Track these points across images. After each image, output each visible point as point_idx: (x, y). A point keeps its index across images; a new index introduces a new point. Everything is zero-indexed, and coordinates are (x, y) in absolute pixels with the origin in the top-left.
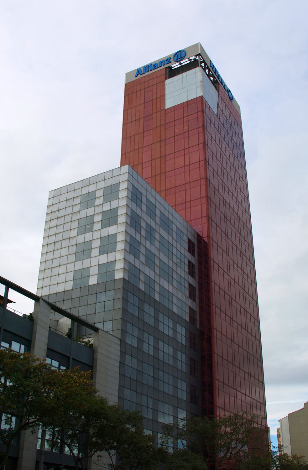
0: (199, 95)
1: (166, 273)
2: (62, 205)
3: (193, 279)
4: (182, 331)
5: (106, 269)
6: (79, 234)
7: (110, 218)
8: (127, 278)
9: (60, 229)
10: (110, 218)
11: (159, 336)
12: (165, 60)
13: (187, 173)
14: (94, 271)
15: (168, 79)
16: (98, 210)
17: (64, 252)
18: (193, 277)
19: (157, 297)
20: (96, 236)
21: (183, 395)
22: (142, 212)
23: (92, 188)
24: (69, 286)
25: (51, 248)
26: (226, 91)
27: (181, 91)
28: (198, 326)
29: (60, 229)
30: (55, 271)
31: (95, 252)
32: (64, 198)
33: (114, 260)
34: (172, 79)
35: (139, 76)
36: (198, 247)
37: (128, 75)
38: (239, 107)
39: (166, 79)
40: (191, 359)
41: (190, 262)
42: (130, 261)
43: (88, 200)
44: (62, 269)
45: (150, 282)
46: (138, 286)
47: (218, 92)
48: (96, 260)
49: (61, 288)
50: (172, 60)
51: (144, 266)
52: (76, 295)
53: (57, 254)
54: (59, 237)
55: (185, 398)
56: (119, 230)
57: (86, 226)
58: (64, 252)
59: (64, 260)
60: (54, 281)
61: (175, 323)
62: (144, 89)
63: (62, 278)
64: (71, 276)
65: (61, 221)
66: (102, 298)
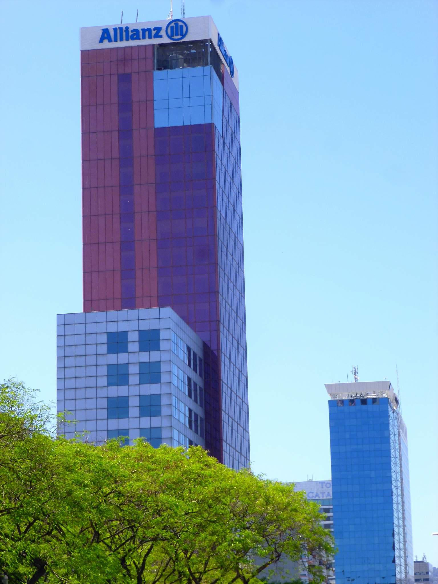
6: (109, 384)
12: (152, 28)
16: (134, 358)
35: (107, 45)
39: (154, 70)
50: (163, 33)
57: (118, 375)
59: (92, 414)
65: (81, 361)
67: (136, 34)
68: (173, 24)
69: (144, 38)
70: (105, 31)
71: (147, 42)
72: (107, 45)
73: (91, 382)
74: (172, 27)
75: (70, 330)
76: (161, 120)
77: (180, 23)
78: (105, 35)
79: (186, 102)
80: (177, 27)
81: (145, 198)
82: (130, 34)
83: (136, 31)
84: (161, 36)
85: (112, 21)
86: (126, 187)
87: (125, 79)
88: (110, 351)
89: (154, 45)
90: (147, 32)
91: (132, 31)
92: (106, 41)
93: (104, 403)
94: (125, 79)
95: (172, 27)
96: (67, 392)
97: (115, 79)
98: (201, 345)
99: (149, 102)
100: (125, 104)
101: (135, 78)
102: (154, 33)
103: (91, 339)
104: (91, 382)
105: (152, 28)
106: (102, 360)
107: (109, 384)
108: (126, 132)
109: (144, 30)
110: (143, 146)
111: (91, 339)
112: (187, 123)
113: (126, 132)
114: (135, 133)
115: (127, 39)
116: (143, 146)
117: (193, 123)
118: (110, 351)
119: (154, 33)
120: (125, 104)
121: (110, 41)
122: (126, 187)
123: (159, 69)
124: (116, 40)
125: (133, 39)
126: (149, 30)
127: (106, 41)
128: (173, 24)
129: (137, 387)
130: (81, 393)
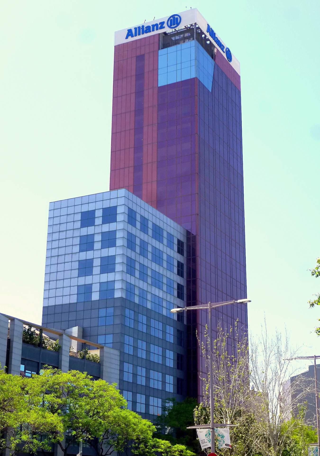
0: (193, 76)
1: (157, 282)
2: (64, 219)
3: (181, 256)
4: (170, 330)
5: (107, 289)
6: (81, 251)
7: (109, 240)
8: (124, 297)
9: (62, 243)
10: (109, 240)
11: (149, 339)
12: (158, 23)
13: (179, 72)
14: (96, 288)
15: (162, 49)
16: (98, 230)
17: (68, 266)
18: (181, 254)
19: (149, 306)
20: (97, 254)
21: (170, 363)
22: (136, 231)
23: (91, 207)
24: (74, 299)
25: (54, 260)
26: (224, 53)
27: (175, 67)
28: (185, 323)
29: (62, 243)
30: (60, 284)
31: (96, 270)
32: (64, 212)
33: (113, 280)
34: (165, 49)
35: (130, 39)
36: (187, 289)
37: (117, 34)
38: (238, 78)
39: (159, 49)
40: (178, 330)
41: (179, 285)
42: (127, 281)
43: (88, 219)
44: (67, 283)
45: (143, 294)
46: (133, 301)
47: (215, 60)
48: (97, 279)
49: (66, 301)
50: (165, 25)
51: (138, 280)
52: (80, 307)
53: (61, 267)
54: (62, 251)
55: (172, 391)
56: (117, 251)
57: (87, 243)
58: (68, 266)
59: (68, 274)
60: (59, 292)
61: (164, 324)
62: (136, 58)
63: (67, 291)
64: (75, 290)
65: (63, 235)
66: (102, 313)
67: (148, 29)
68: (172, 18)
69: (153, 30)
70: (130, 31)
71: (156, 32)
72: (130, 39)
73: (69, 250)
74: (171, 20)
75: (57, 213)
76: (162, 81)
77: (176, 17)
78: (130, 33)
79: (179, 66)
80: (174, 20)
81: (150, 134)
82: (145, 29)
83: (148, 27)
84: (164, 27)
85: (133, 25)
86: (138, 129)
87: (140, 58)
88: (82, 226)
89: (159, 34)
90: (156, 26)
91: (146, 28)
92: (130, 37)
93: (76, 265)
94: (140, 58)
95: (171, 20)
96: (53, 258)
97: (134, 60)
98: (184, 232)
99: (155, 71)
100: (140, 75)
101: (146, 57)
102: (159, 26)
103: (70, 218)
104: (69, 250)
105: (158, 23)
106: (77, 233)
107: (81, 251)
108: (140, 93)
109: (153, 26)
110: (150, 100)
111: (70, 218)
112: (179, 80)
113: (140, 93)
114: (146, 93)
115: (143, 33)
116: (150, 100)
117: (183, 79)
118: (82, 226)
119: (159, 26)
120: (140, 75)
121: (132, 36)
122: (138, 129)
123: (163, 48)
124: (136, 35)
125: (146, 32)
126: (157, 25)
127: (130, 37)
128: (172, 18)
129: (100, 251)
130: (61, 259)
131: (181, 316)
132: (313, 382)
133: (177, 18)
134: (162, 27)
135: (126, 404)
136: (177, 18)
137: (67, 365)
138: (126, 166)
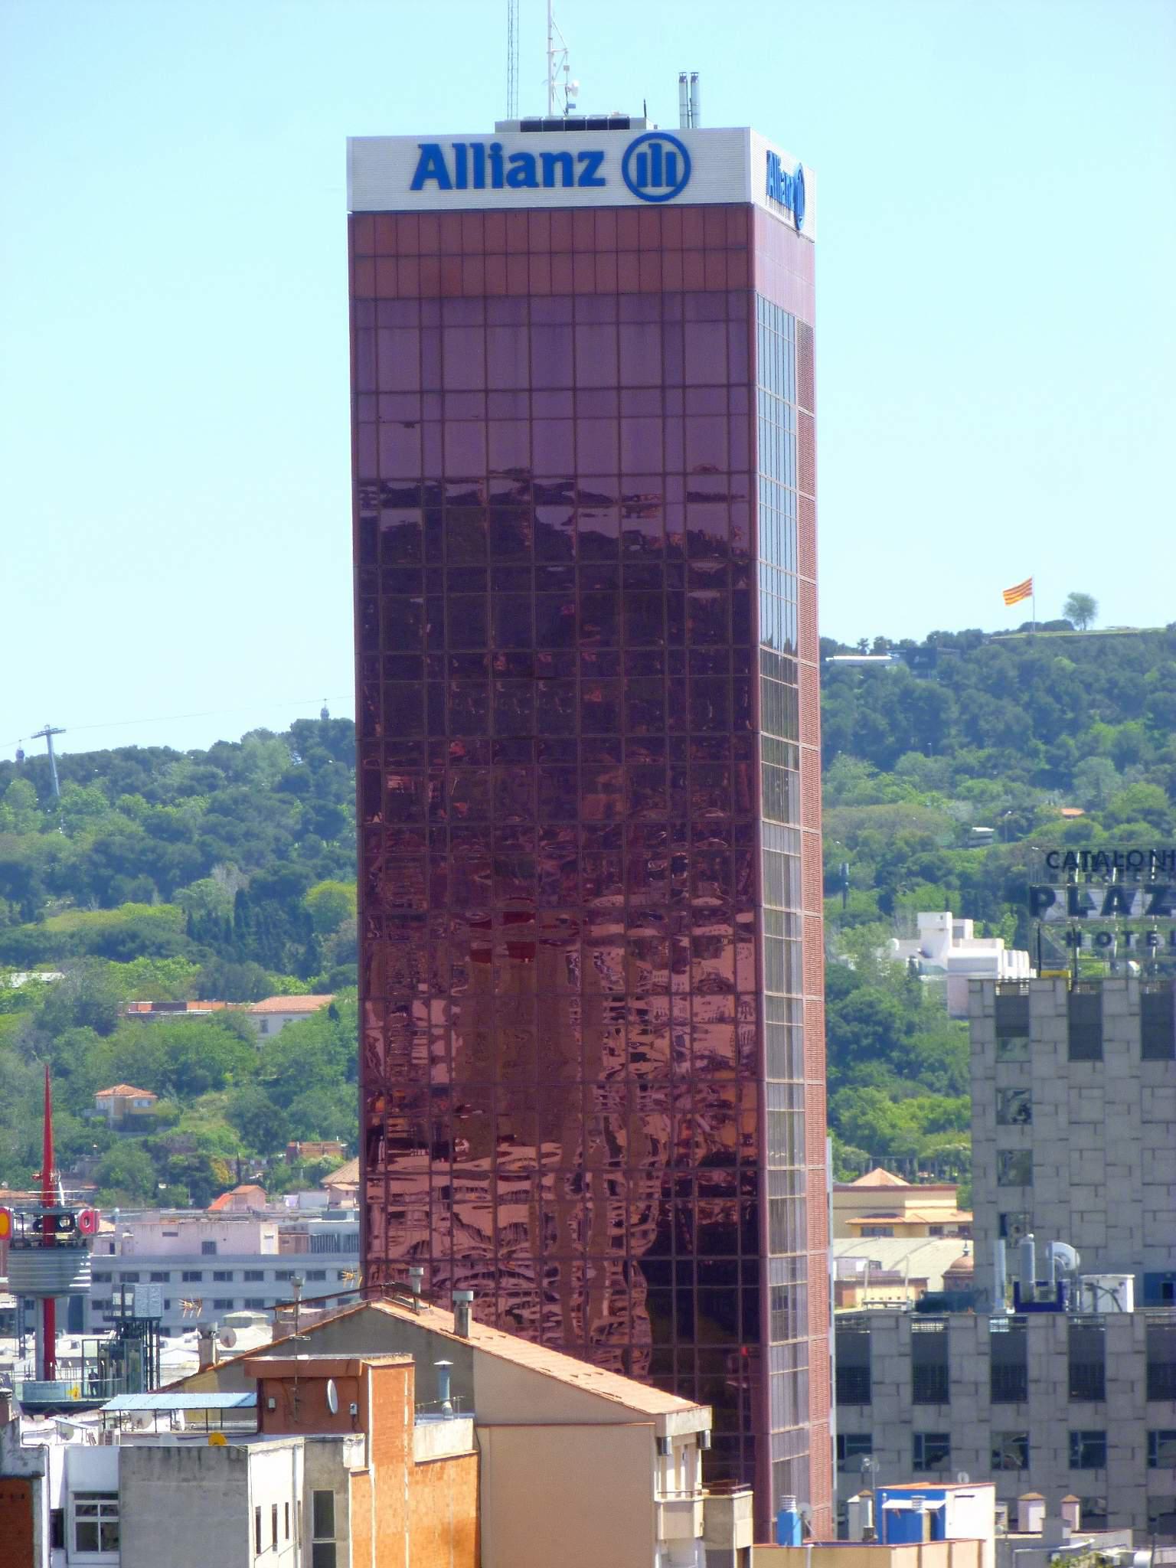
35: (433, 198)
74: (642, 158)
77: (668, 147)
84: (601, 182)
91: (514, 158)
92: (431, 185)
102: (579, 168)
119: (579, 168)
124: (462, 184)
125: (514, 183)
127: (431, 185)
128: (644, 148)
131: (197, 763)
132: (764, 644)
133: (671, 157)
134: (589, 179)
135: (48, 1057)
136: (671, 157)
137: (1133, 1029)
138: (336, 721)
